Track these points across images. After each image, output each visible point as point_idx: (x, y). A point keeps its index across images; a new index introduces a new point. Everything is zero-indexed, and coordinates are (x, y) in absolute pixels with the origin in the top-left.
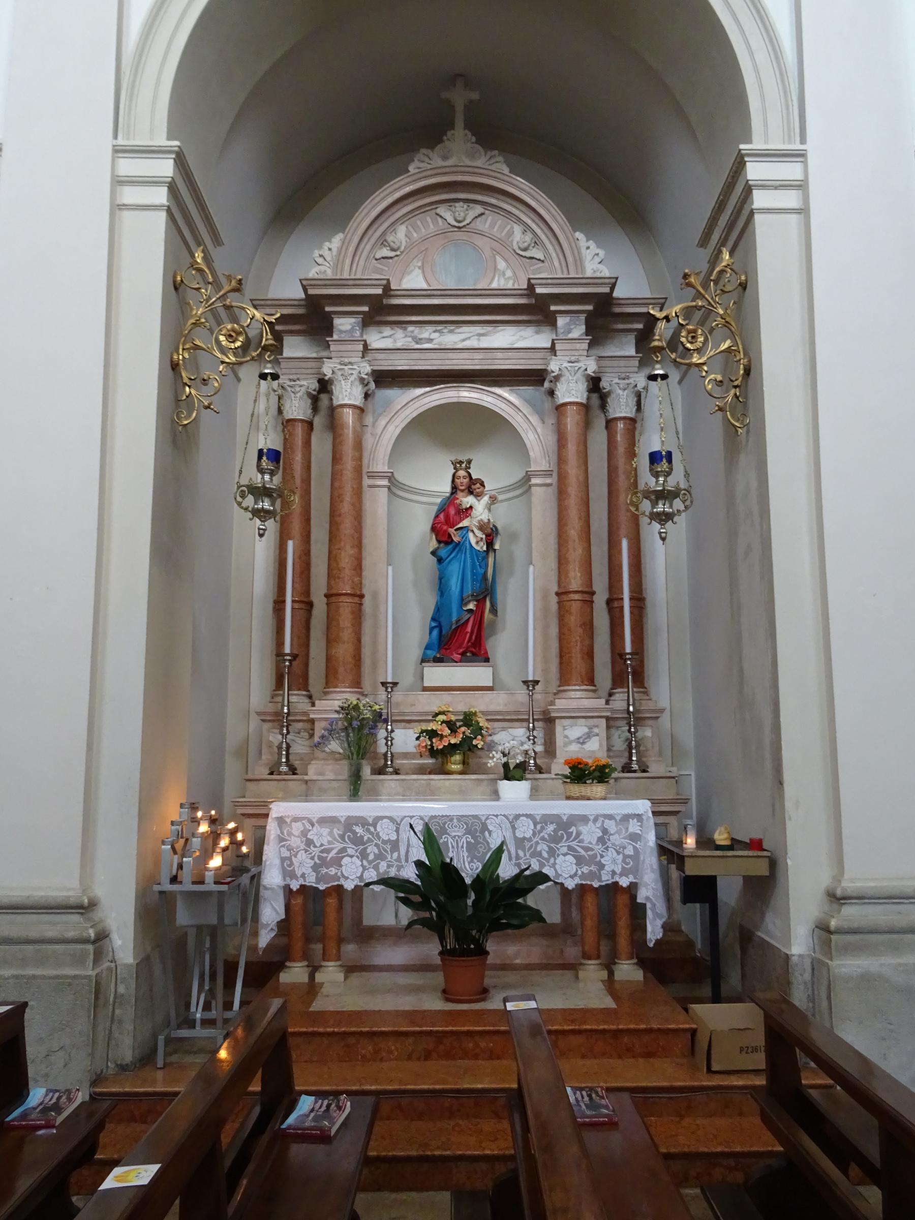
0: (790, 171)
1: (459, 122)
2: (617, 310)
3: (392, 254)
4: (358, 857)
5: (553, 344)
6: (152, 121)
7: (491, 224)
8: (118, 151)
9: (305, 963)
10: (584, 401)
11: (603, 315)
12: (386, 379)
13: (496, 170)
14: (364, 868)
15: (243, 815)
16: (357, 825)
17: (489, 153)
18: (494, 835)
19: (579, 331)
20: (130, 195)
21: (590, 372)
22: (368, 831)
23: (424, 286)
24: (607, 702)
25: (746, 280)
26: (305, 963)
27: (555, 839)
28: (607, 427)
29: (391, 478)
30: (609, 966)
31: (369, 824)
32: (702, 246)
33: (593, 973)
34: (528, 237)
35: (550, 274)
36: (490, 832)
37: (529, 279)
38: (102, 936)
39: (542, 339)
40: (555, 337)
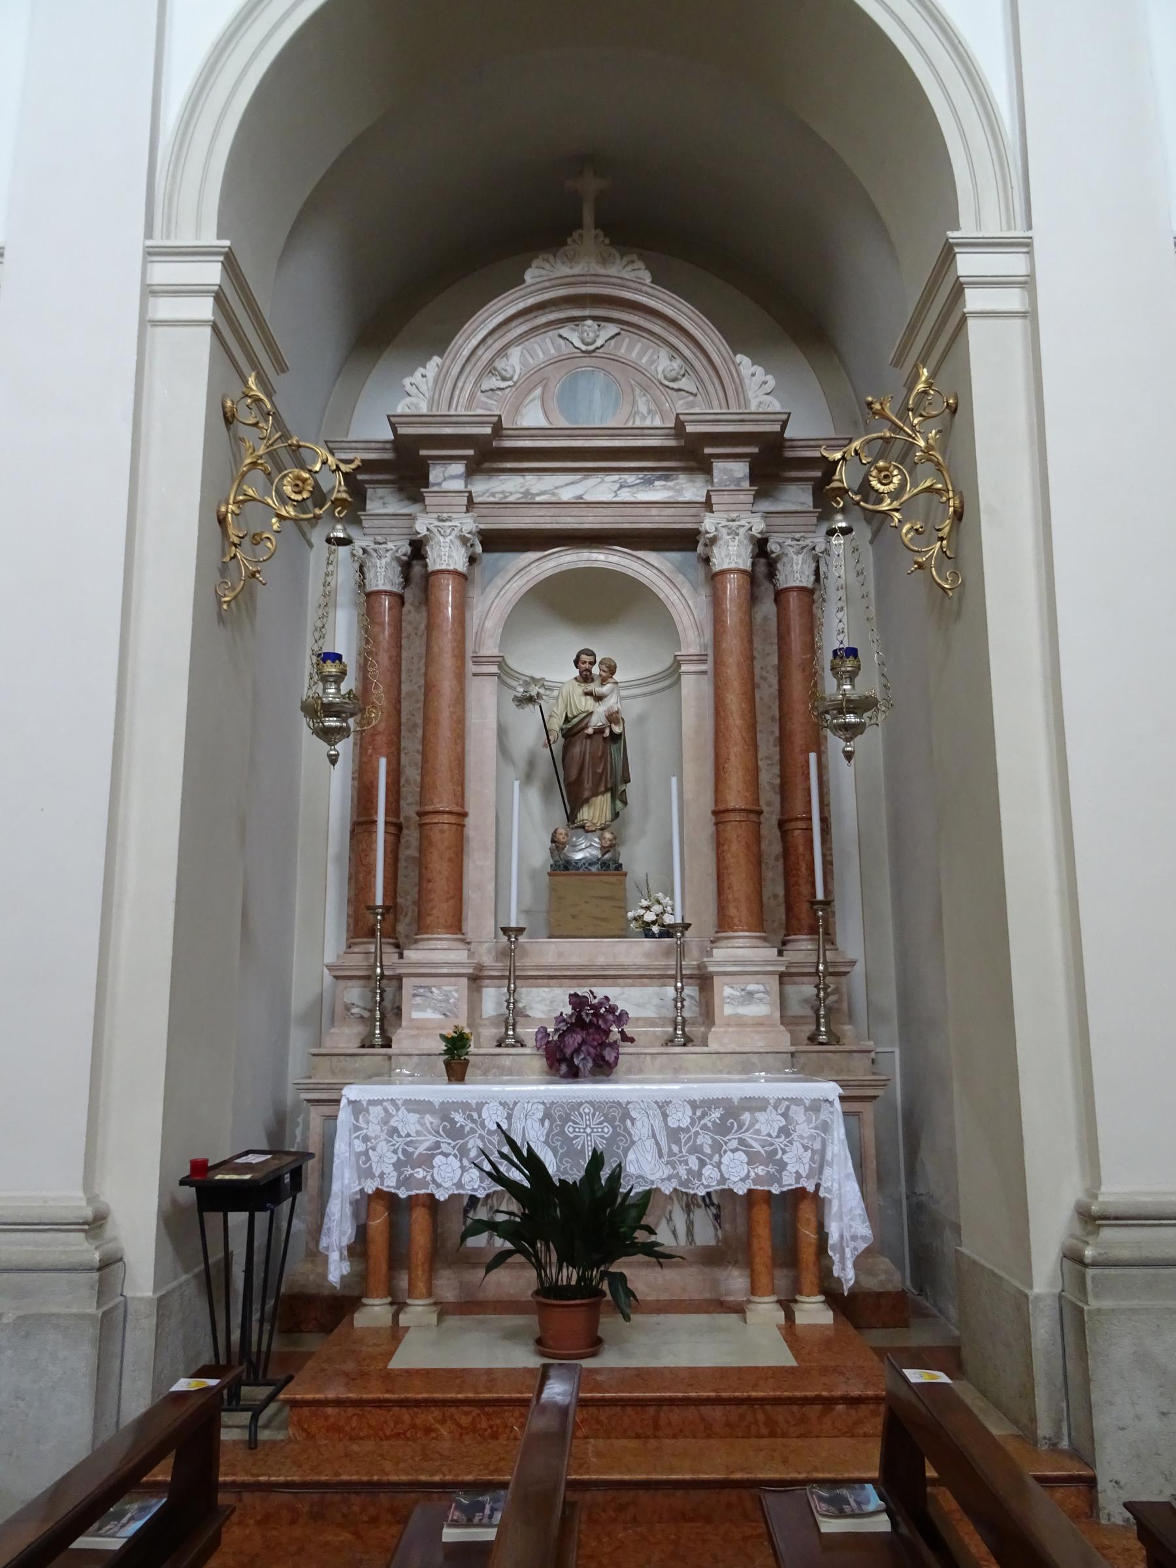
0: (1012, 264)
1: (588, 218)
2: (789, 454)
3: (503, 384)
4: (455, 1156)
5: (709, 497)
6: (199, 218)
7: (634, 350)
8: (152, 253)
9: (389, 1300)
10: (747, 566)
11: (771, 461)
12: (497, 541)
13: (632, 279)
14: (463, 1168)
15: (309, 1101)
16: (456, 1111)
17: (625, 260)
18: (638, 1124)
19: (740, 469)
20: (164, 308)
21: (754, 532)
22: (470, 1117)
23: (544, 423)
24: (780, 953)
25: (957, 404)
26: (389, 1300)
27: (722, 1129)
28: (776, 601)
29: (501, 663)
30: (787, 1306)
31: (472, 1110)
32: (896, 366)
33: (766, 1312)
34: (677, 363)
35: (704, 411)
36: (633, 1121)
37: (678, 415)
38: (109, 1264)
39: (690, 489)
40: (710, 488)
